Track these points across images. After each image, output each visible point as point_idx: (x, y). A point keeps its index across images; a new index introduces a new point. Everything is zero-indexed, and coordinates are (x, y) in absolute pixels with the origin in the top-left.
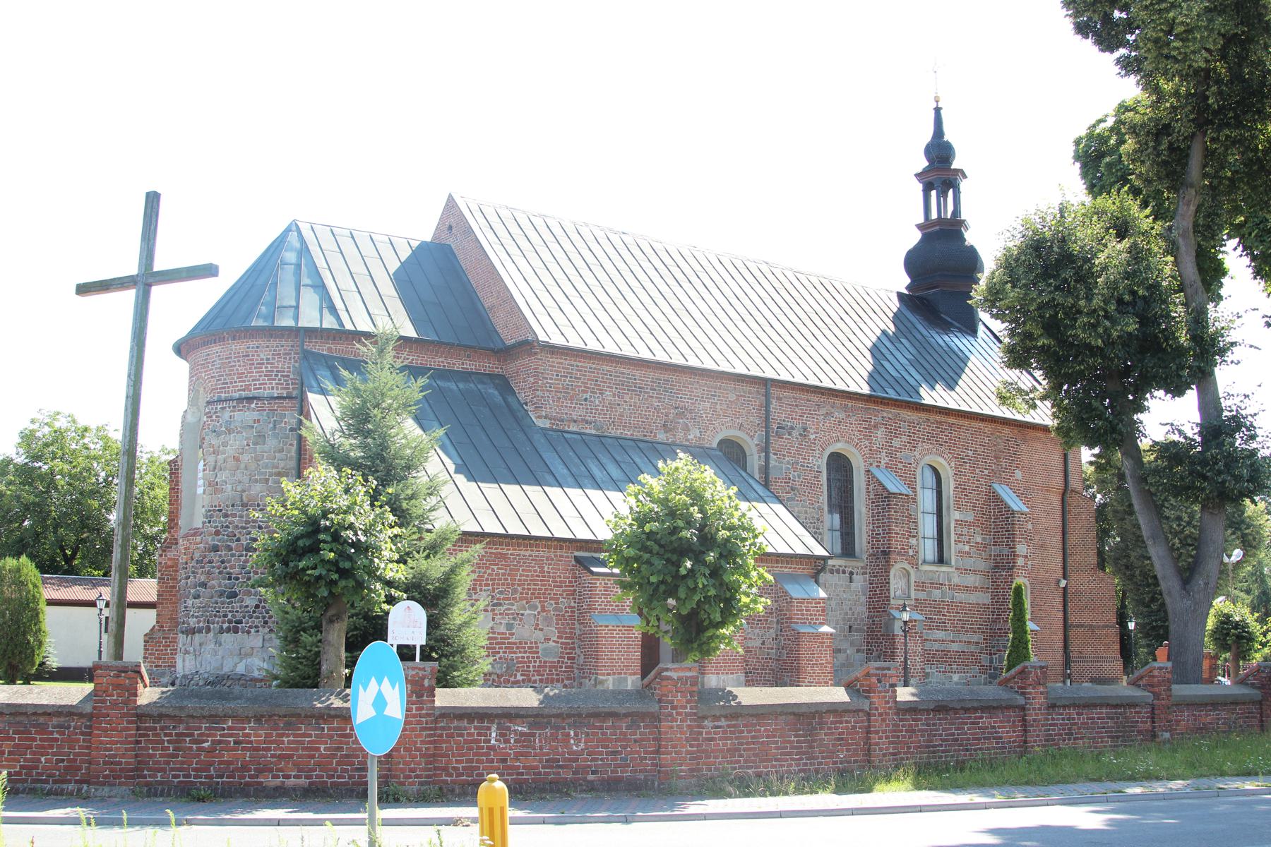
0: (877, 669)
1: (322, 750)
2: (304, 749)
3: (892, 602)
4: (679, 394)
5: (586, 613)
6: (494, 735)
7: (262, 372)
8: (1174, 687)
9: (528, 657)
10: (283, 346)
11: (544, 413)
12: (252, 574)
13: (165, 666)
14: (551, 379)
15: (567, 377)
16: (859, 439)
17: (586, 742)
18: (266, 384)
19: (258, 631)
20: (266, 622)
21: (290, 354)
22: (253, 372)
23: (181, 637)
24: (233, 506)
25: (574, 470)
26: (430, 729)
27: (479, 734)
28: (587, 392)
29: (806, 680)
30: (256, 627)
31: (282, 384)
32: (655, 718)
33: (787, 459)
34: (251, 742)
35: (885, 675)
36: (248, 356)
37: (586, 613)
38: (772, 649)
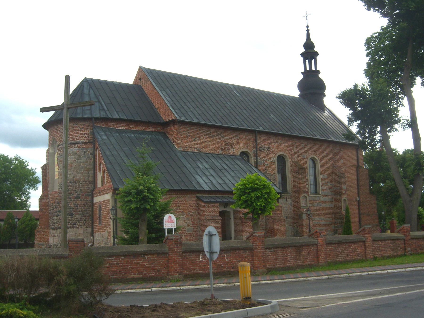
0: (319, 230)
1: (146, 265)
2: (140, 265)
3: (301, 208)
4: (226, 137)
5: (202, 216)
6: (201, 257)
7: (79, 134)
8: (411, 233)
9: (182, 232)
10: (86, 124)
11: (180, 145)
12: (78, 207)
13: (43, 242)
14: (182, 133)
15: (187, 132)
16: (287, 151)
17: (230, 258)
18: (80, 138)
19: (82, 227)
20: (84, 224)
21: (89, 127)
22: (75, 134)
23: (52, 231)
24: (70, 182)
25: (193, 165)
26: (181, 256)
27: (196, 257)
28: (194, 137)
29: (277, 236)
30: (81, 226)
31: (86, 138)
32: (251, 249)
33: (263, 158)
34: (122, 263)
35: (322, 232)
36: (73, 128)
37: (202, 216)
38: (264, 226)
